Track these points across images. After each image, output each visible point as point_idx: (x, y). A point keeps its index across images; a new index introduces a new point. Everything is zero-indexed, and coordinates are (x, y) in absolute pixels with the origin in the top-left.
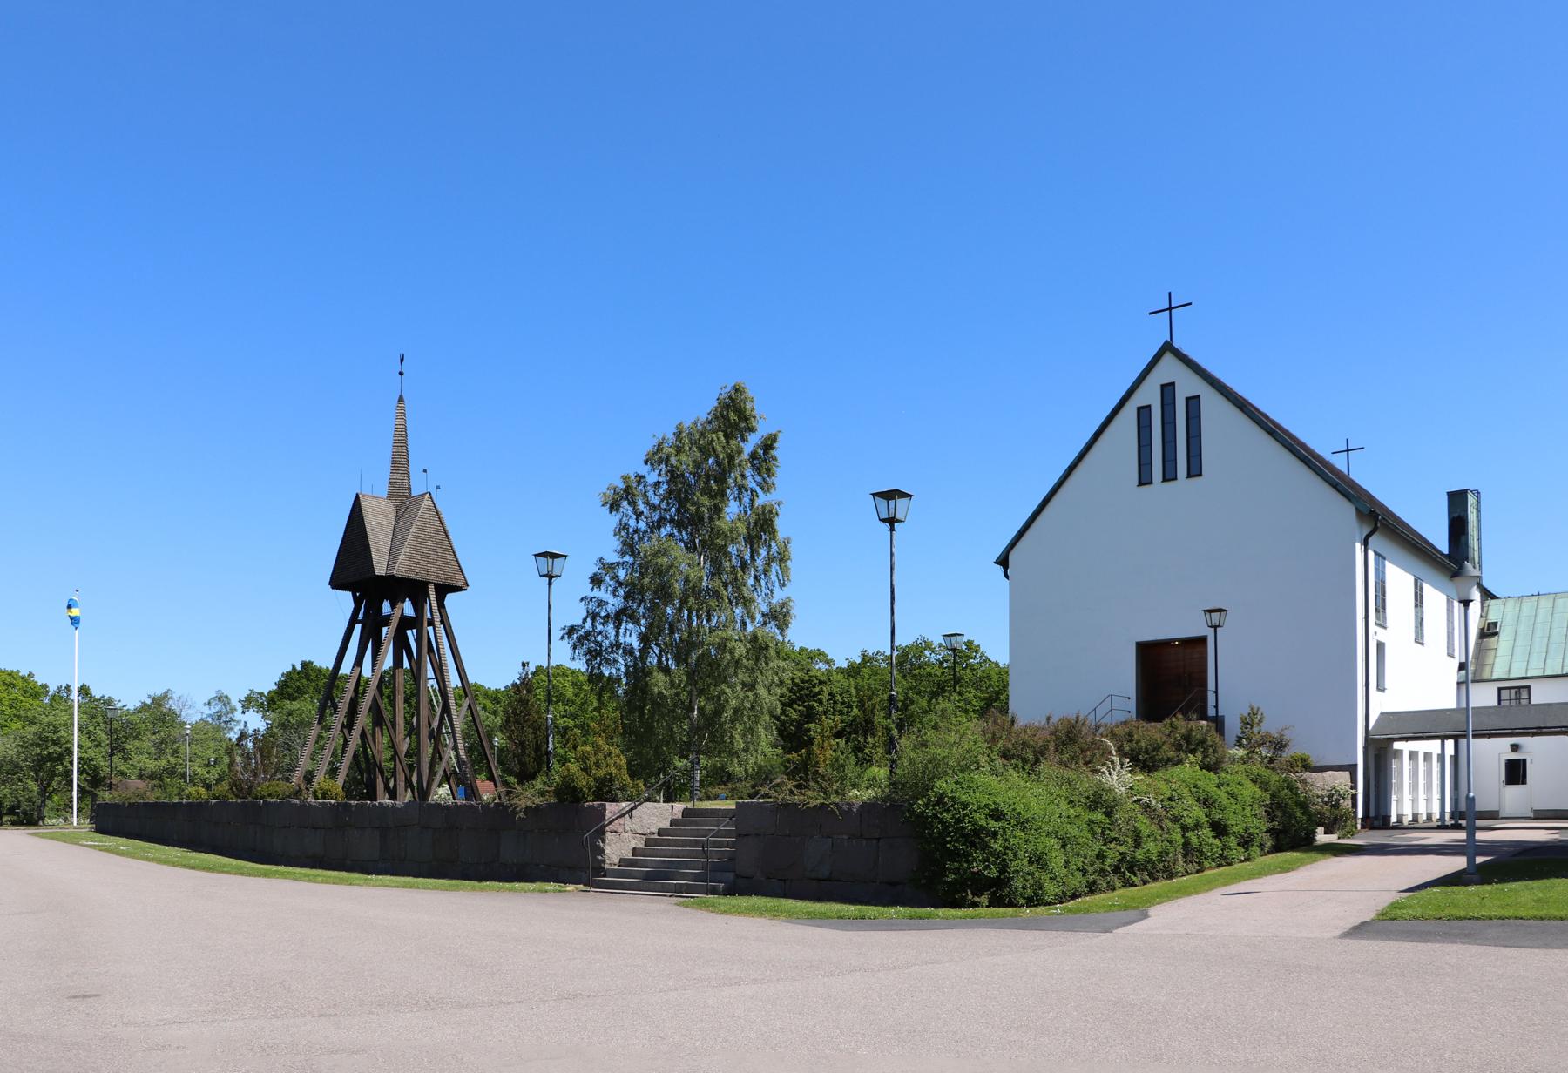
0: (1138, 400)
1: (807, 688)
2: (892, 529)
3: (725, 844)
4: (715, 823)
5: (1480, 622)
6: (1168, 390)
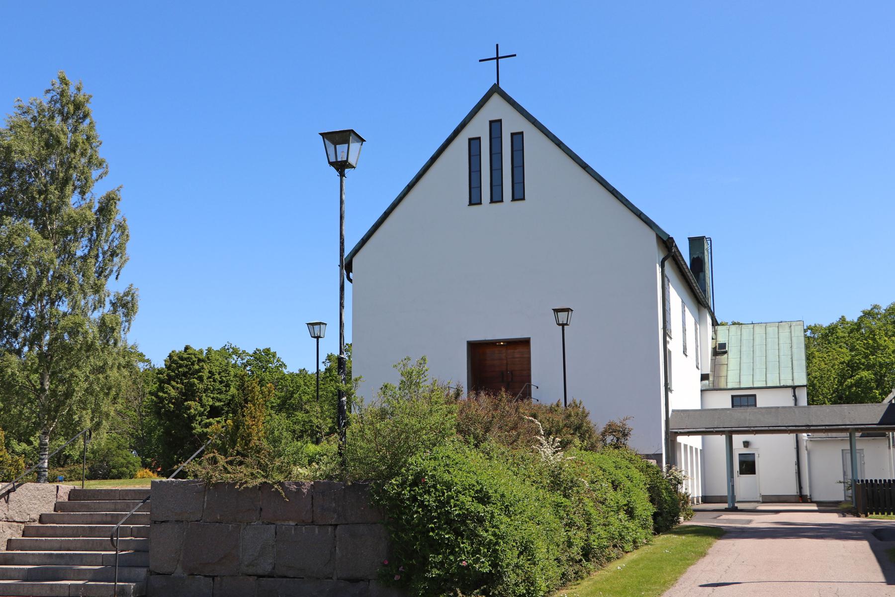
0: (470, 132)
1: (186, 366)
2: (342, 175)
3: (129, 531)
4: (113, 507)
5: (712, 343)
6: (495, 126)
